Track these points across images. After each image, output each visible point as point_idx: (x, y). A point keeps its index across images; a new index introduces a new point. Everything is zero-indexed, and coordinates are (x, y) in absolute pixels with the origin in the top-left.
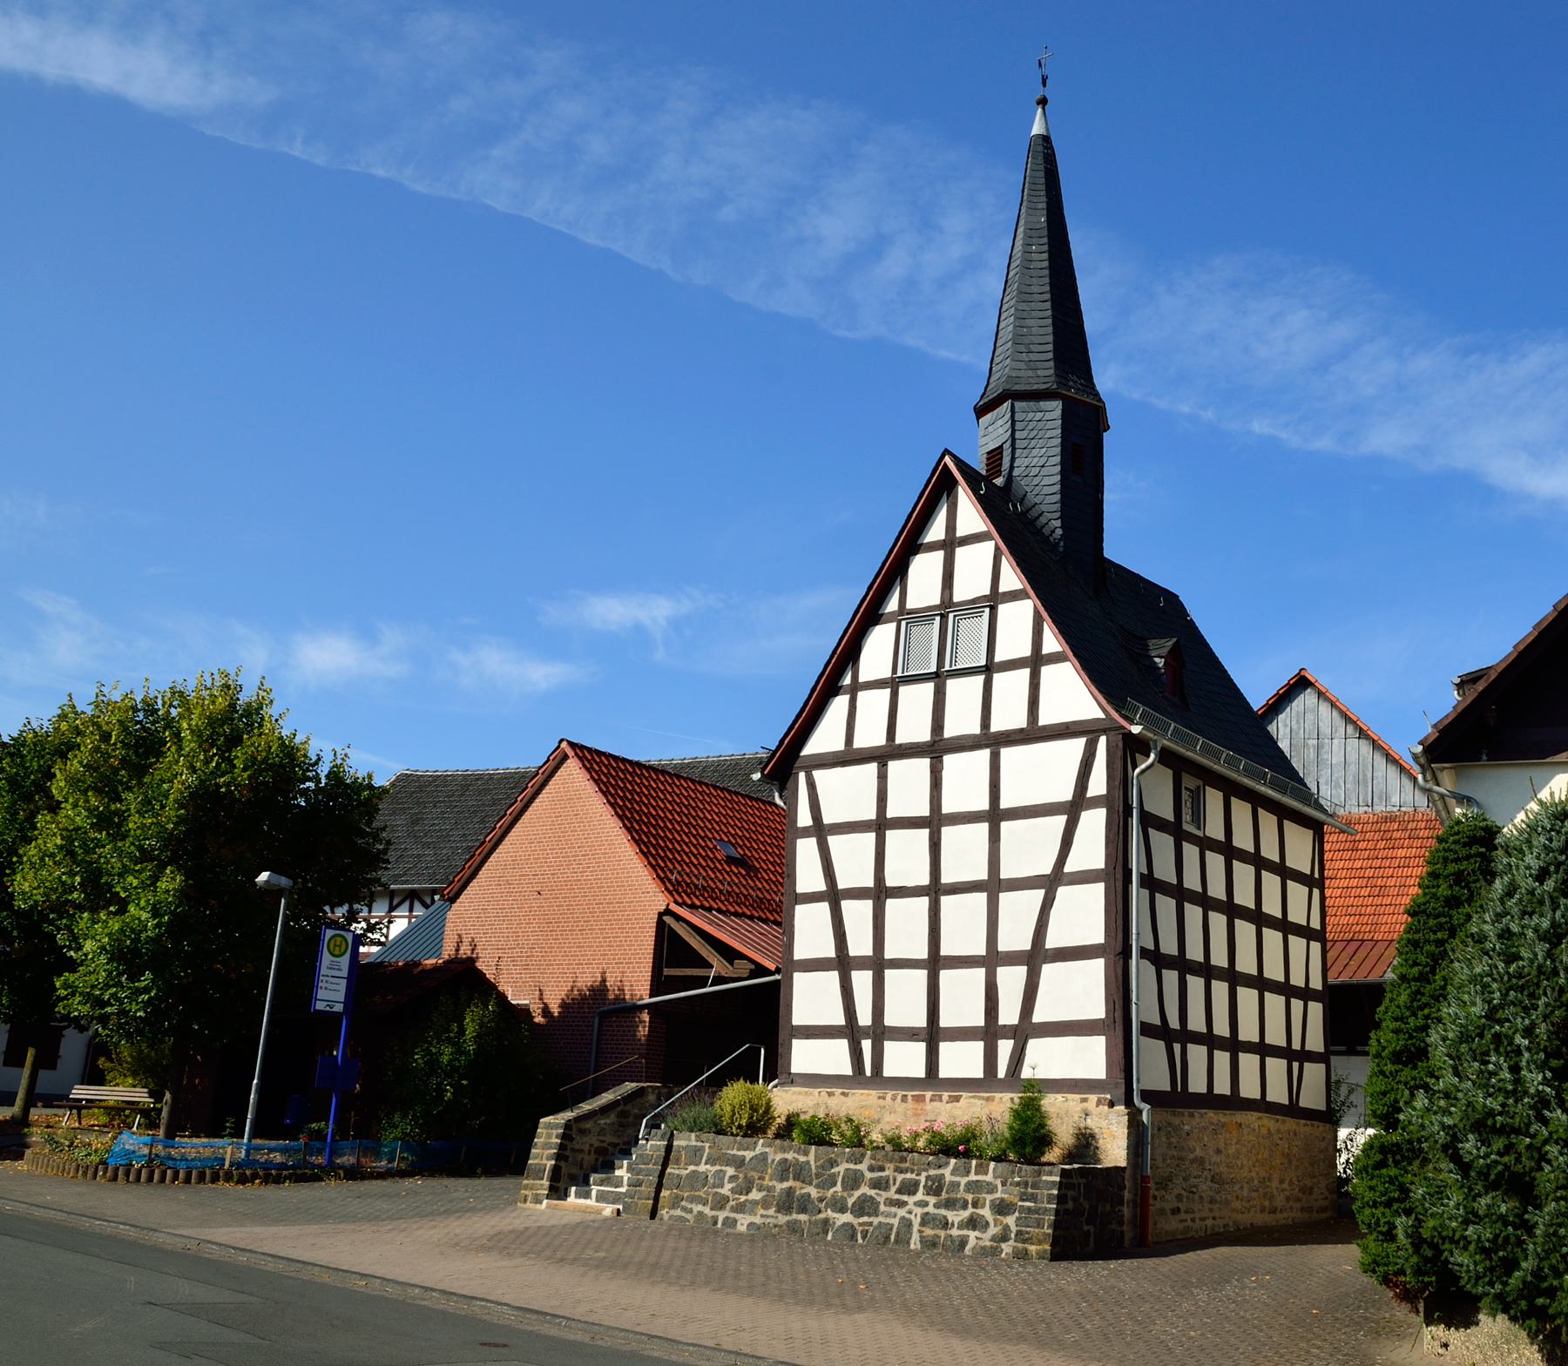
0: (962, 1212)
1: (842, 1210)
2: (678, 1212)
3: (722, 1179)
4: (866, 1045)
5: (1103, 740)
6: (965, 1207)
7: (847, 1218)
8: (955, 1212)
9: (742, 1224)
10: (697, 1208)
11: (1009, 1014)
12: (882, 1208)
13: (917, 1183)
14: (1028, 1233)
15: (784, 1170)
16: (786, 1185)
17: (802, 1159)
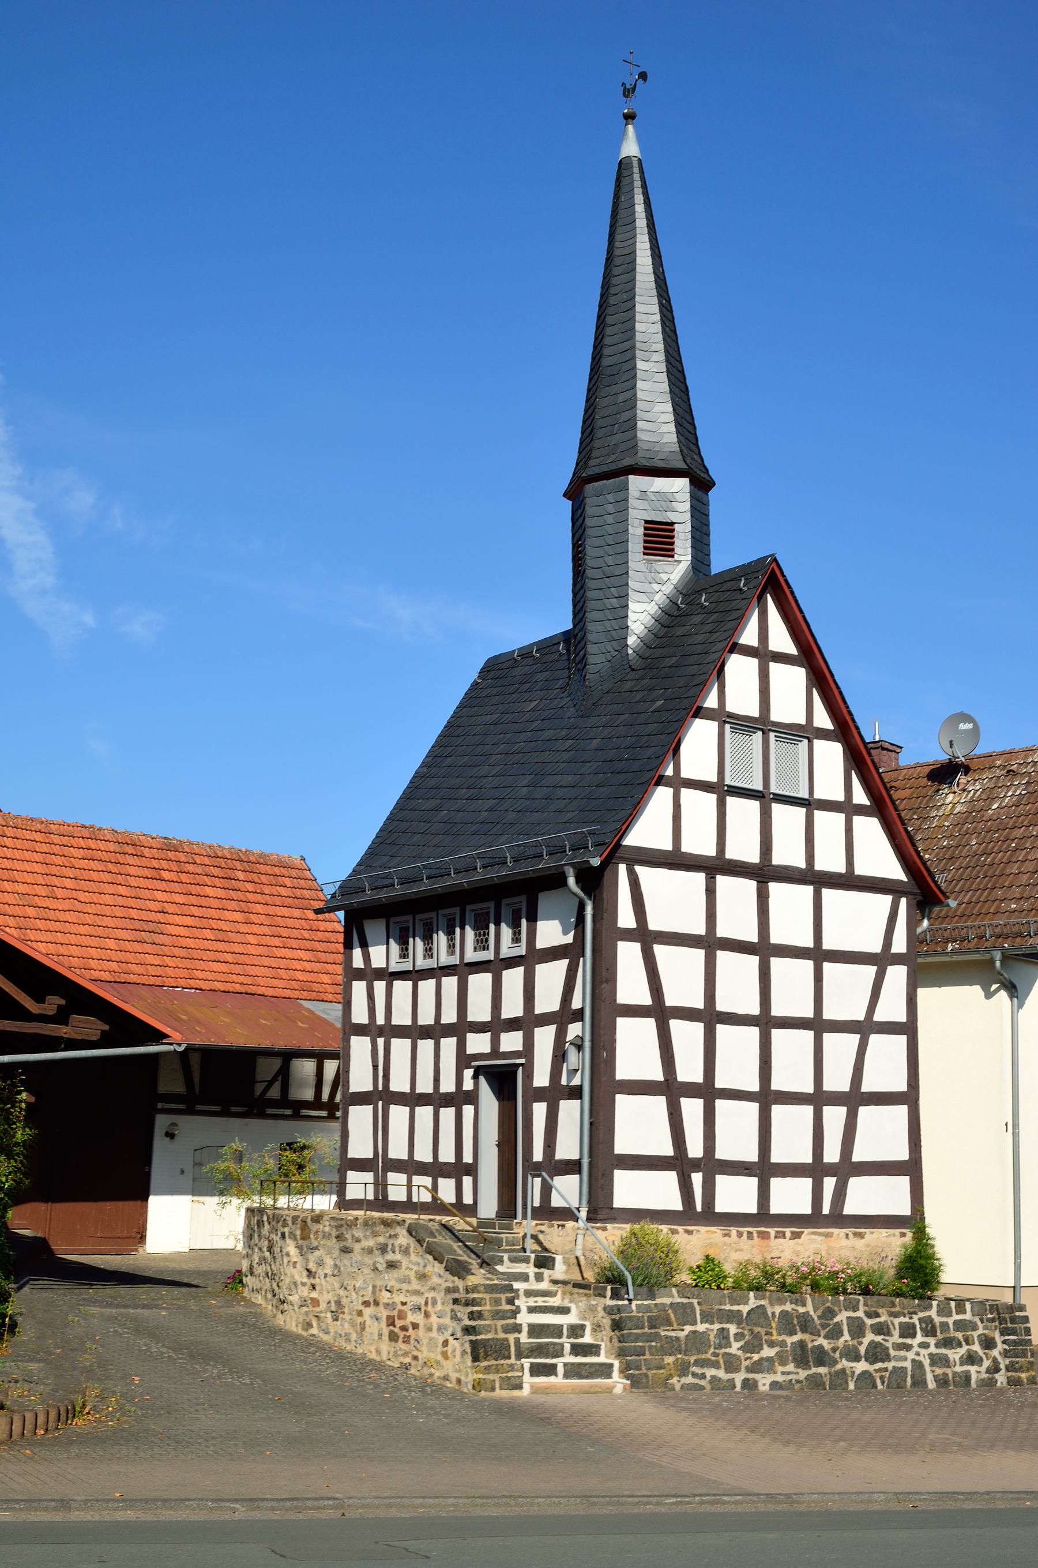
0: (958, 1350)
1: (857, 1358)
2: (689, 1380)
3: (727, 1338)
4: (697, 1178)
5: (903, 901)
6: (960, 1345)
7: (862, 1366)
8: (953, 1351)
9: (764, 1385)
10: (710, 1372)
11: (832, 1154)
12: (892, 1353)
13: (1025, 1328)
14: (1017, 1363)
15: (787, 1323)
16: (795, 1338)
17: (801, 1310)
